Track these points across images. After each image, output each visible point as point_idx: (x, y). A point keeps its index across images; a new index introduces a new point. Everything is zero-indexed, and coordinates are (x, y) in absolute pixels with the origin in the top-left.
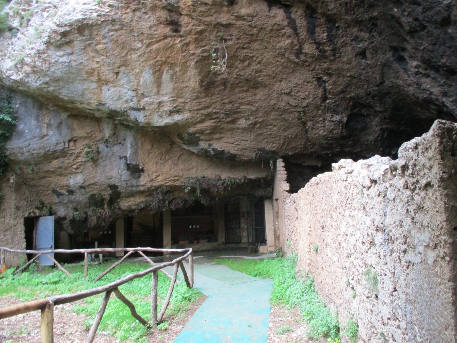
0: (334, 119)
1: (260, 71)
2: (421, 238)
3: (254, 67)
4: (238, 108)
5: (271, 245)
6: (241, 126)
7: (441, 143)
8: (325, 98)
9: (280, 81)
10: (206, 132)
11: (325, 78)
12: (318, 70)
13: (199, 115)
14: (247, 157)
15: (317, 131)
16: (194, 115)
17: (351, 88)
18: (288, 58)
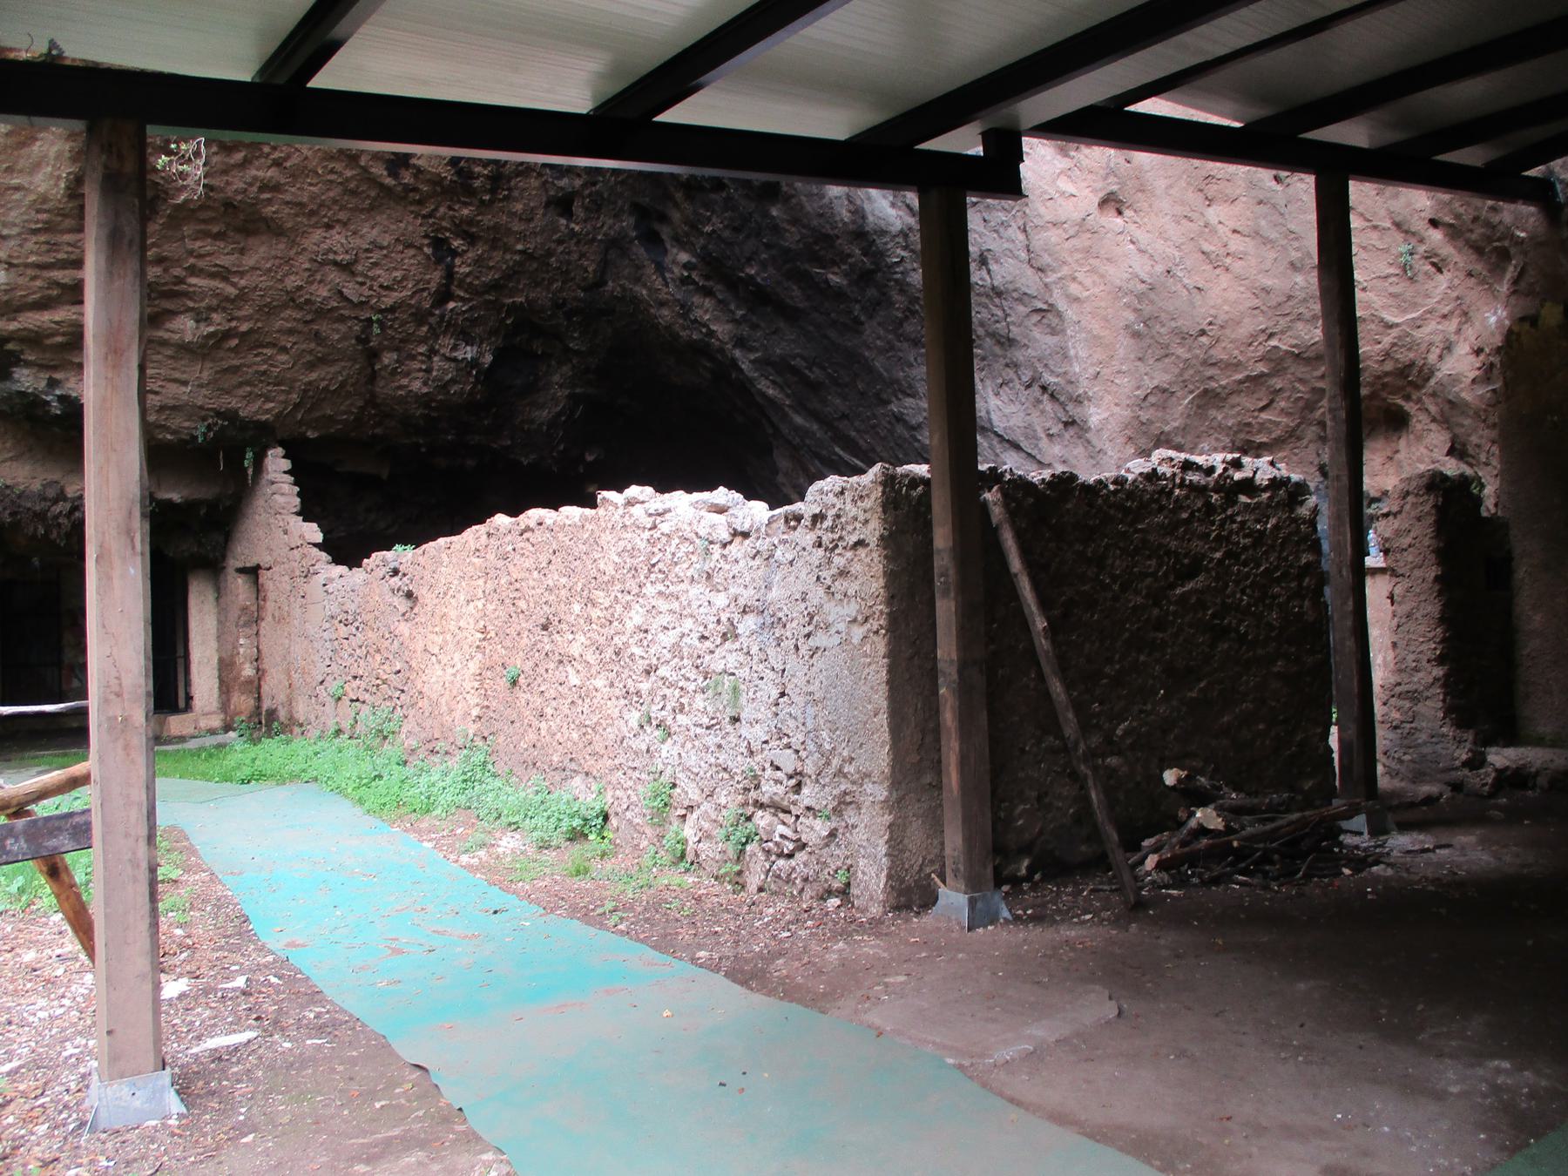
0: (459, 355)
1: (277, 188)
2: (839, 613)
3: (260, 174)
4: (180, 281)
5: (206, 710)
6: (177, 337)
7: (884, 493)
8: (443, 296)
9: (329, 227)
10: (48, 342)
11: (456, 243)
12: (442, 218)
13: (38, 283)
14: (174, 432)
15: (405, 382)
16: (21, 281)
17: (518, 282)
18: (365, 169)
